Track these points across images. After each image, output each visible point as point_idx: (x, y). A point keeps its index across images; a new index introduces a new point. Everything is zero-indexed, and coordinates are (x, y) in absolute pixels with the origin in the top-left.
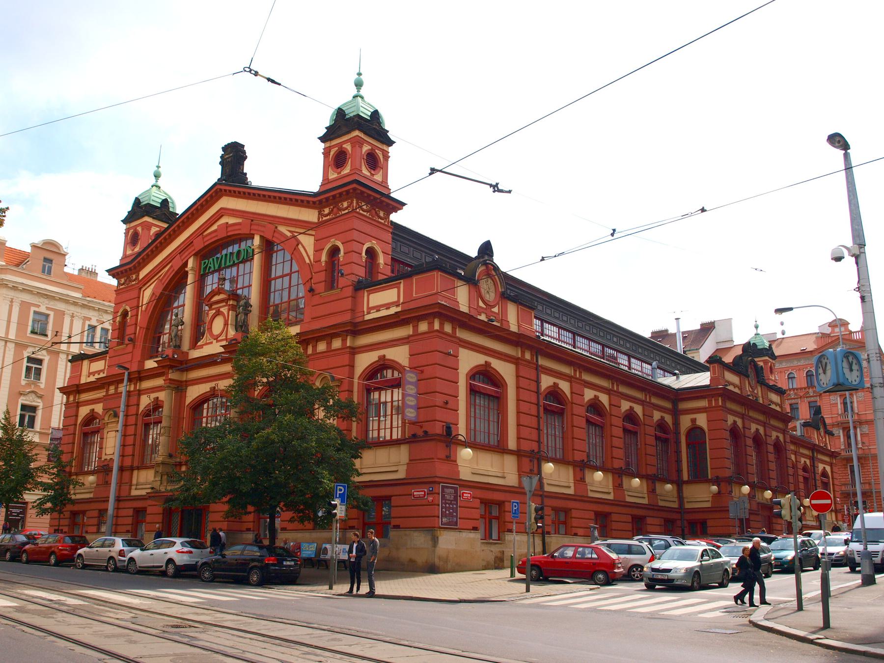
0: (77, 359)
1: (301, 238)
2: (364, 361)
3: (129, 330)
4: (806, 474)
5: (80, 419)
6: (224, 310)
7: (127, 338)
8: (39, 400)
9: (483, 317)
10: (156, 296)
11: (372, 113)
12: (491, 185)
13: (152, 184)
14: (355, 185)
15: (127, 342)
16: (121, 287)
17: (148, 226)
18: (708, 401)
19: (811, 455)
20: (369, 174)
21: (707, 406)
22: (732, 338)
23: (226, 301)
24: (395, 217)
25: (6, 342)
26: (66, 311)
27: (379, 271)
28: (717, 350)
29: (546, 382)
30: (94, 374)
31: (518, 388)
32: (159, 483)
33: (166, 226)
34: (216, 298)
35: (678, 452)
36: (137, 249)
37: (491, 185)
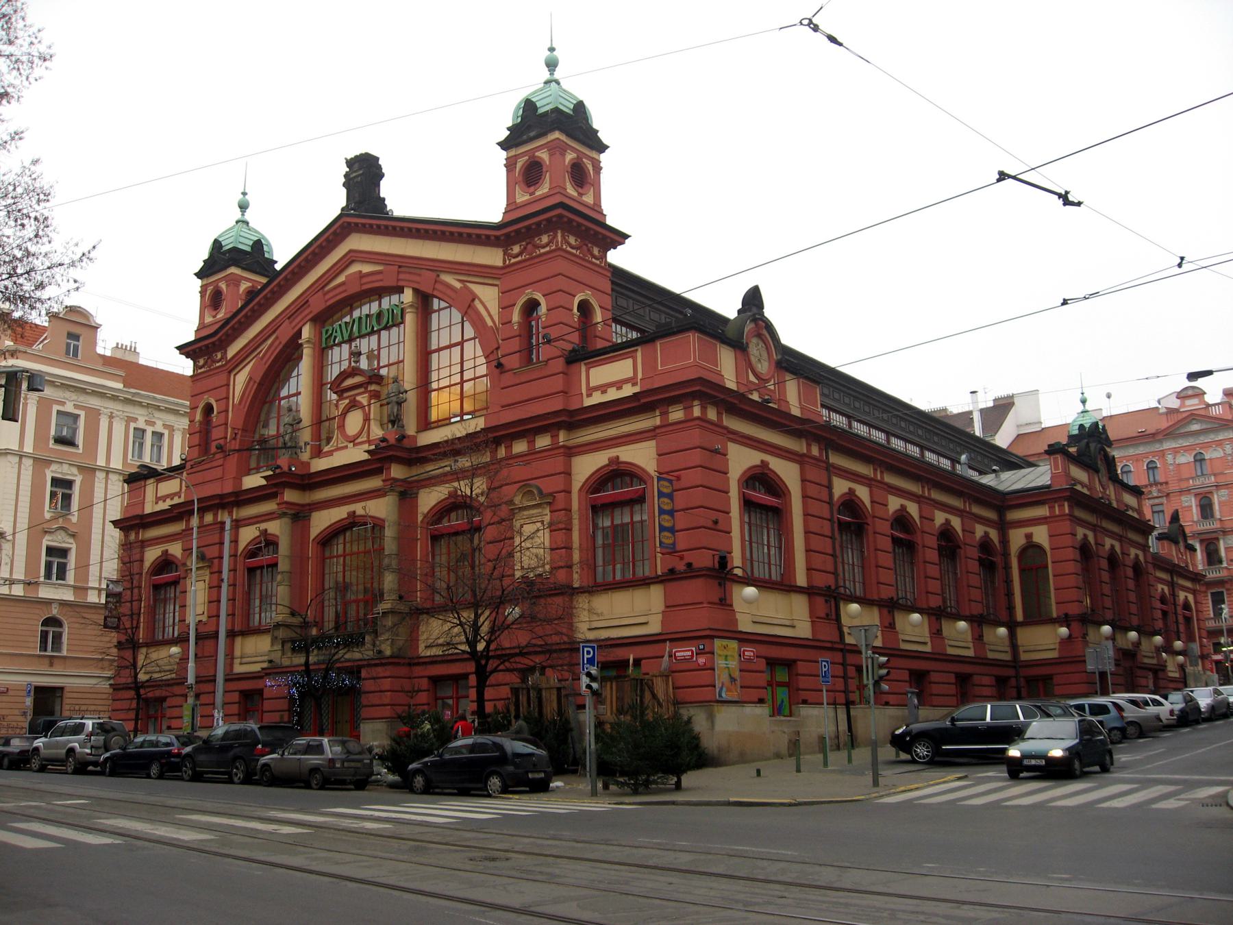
0: (138, 478)
1: (477, 289)
2: (586, 466)
3: (216, 433)
4: (1164, 607)
5: (147, 564)
6: (363, 399)
7: (214, 444)
8: (71, 540)
9: (755, 397)
10: (255, 382)
11: (575, 105)
12: (1060, 196)
13: (236, 219)
14: (559, 211)
15: (213, 450)
16: (199, 371)
17: (234, 281)
18: (1049, 507)
19: (1170, 579)
20: (575, 194)
21: (1048, 514)
22: (1040, 418)
23: (365, 386)
24: (615, 257)
25: (21, 457)
26: (102, 409)
27: (598, 334)
28: (1018, 435)
29: (840, 487)
30: (164, 498)
31: (805, 497)
32: (280, 653)
33: (264, 280)
34: (350, 382)
35: (1008, 581)
36: (220, 315)
37: (1060, 196)
